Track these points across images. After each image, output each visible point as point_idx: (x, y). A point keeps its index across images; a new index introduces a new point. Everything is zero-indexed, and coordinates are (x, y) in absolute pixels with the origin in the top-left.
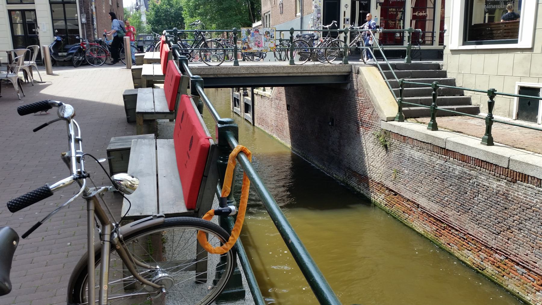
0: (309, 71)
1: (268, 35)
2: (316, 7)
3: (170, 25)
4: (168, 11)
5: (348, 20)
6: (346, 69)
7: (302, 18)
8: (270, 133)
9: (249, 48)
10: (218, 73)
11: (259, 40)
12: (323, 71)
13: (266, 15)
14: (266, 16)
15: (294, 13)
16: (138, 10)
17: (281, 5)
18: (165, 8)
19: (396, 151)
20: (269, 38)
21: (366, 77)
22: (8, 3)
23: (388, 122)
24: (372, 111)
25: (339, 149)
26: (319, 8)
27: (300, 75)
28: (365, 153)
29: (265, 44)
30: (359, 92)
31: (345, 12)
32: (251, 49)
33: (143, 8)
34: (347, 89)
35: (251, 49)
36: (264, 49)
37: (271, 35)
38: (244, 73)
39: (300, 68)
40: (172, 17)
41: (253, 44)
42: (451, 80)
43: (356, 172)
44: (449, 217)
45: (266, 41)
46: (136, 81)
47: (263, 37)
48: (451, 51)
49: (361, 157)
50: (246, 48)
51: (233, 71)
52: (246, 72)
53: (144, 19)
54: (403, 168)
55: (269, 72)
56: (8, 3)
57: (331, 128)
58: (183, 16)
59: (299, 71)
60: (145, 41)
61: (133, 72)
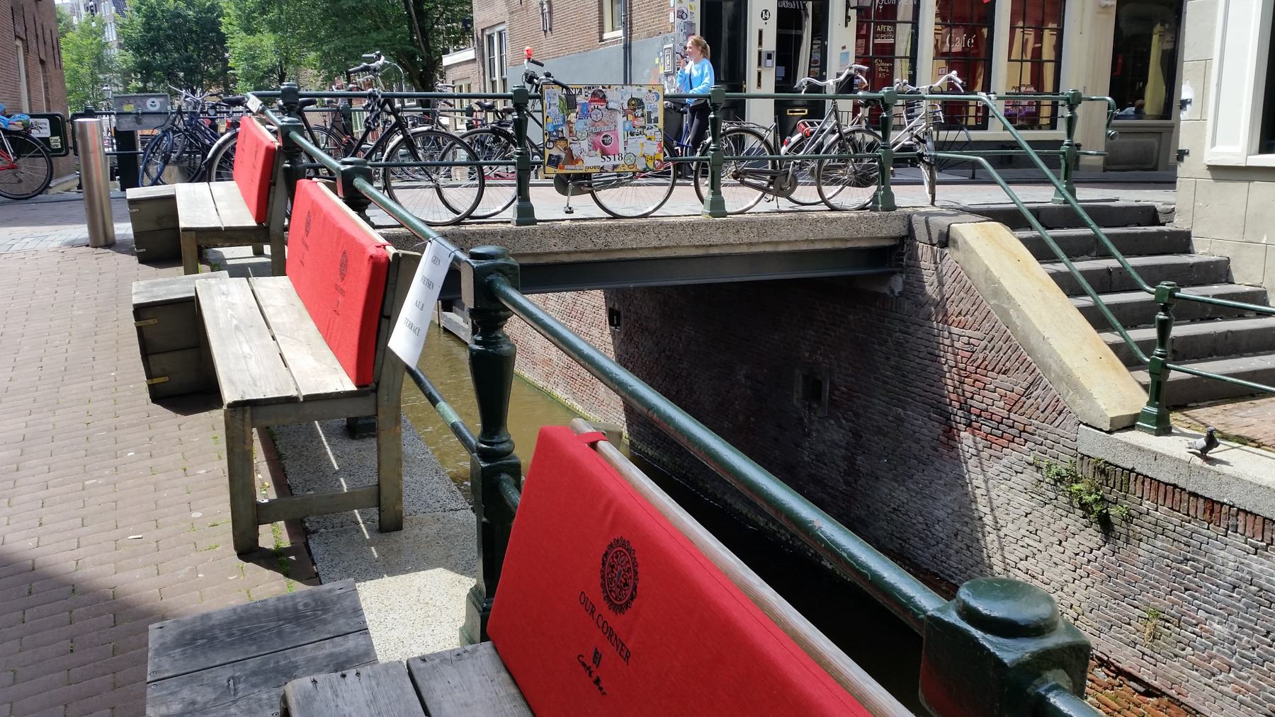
0: (775, 239)
1: (639, 112)
2: (681, 15)
3: (186, 51)
4: (179, 15)
5: (769, 57)
6: (885, 229)
7: (627, 48)
8: (540, 384)
9: (571, 159)
12: (820, 237)
13: (487, 32)
14: (490, 38)
15: (595, 31)
16: (92, 11)
17: (545, 6)
18: (172, 8)
19: (1159, 544)
20: (641, 122)
21: (986, 262)
23: (1117, 436)
24: (1025, 384)
25: (847, 483)
26: (688, 19)
27: (744, 250)
28: (988, 520)
29: (626, 142)
30: (952, 309)
31: (761, 32)
33: (107, 7)
34: (886, 291)
35: (580, 163)
36: (622, 162)
37: (649, 113)
38: (556, 249)
39: (747, 229)
40: (190, 31)
41: (585, 144)
42: (1208, 263)
43: (937, 575)
45: (632, 134)
46: (158, 361)
47: (620, 119)
48: (1214, 169)
49: (968, 530)
50: (559, 157)
51: (518, 246)
52: (564, 249)
53: (111, 35)
54: (1201, 614)
55: (643, 245)
57: (810, 407)
58: (223, 30)
59: (745, 237)
60: (143, 114)
61: (142, 323)
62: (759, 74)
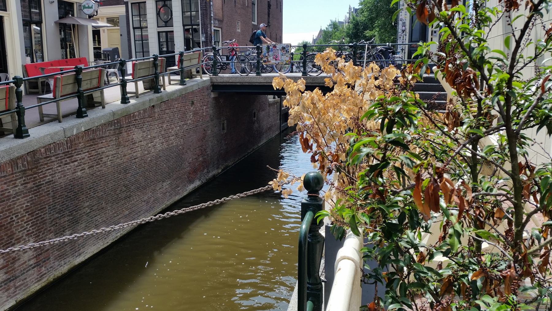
9: (268, 61)
10: (243, 81)
11: (276, 54)
20: (285, 52)
22: (158, 27)
32: (270, 61)
41: (272, 58)
44: (295, 198)
47: (280, 52)
56: (158, 27)
62: (432, 38)
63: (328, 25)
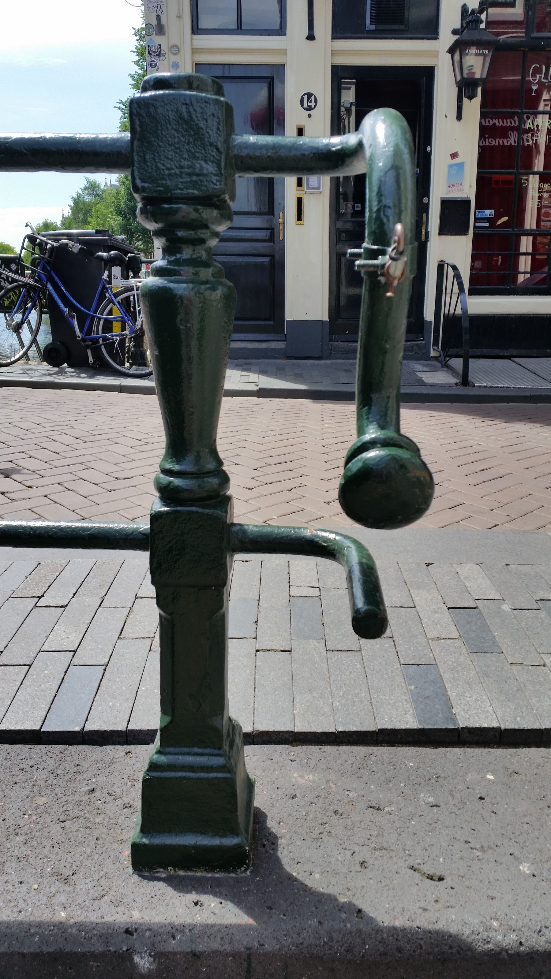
62: (300, 201)
63: (83, 187)
